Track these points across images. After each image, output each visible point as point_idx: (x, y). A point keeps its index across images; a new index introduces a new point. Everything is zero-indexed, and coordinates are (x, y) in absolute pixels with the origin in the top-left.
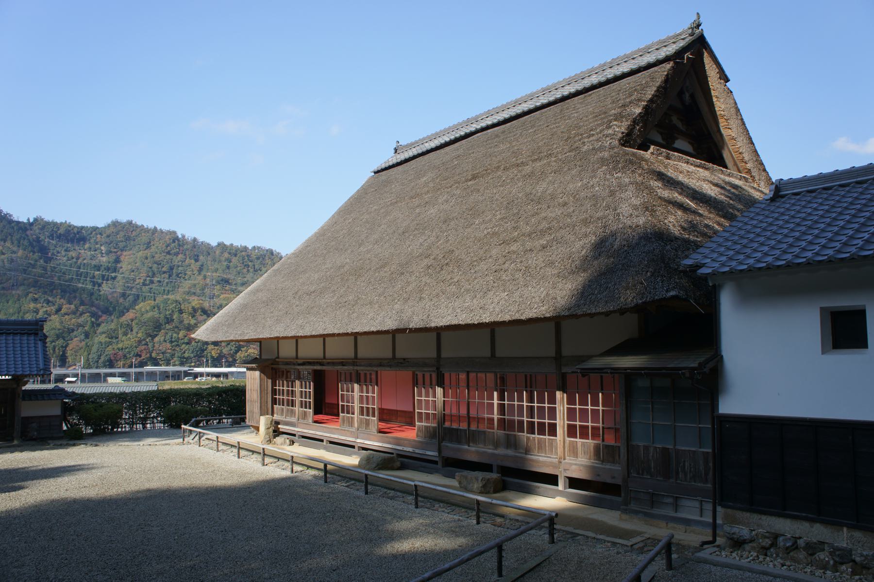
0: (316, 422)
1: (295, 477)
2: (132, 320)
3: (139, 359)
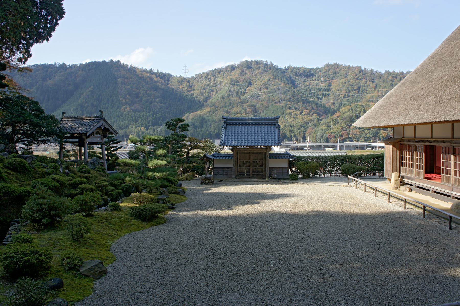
0: (426, 178)
1: (406, 212)
2: (338, 117)
3: (342, 138)
